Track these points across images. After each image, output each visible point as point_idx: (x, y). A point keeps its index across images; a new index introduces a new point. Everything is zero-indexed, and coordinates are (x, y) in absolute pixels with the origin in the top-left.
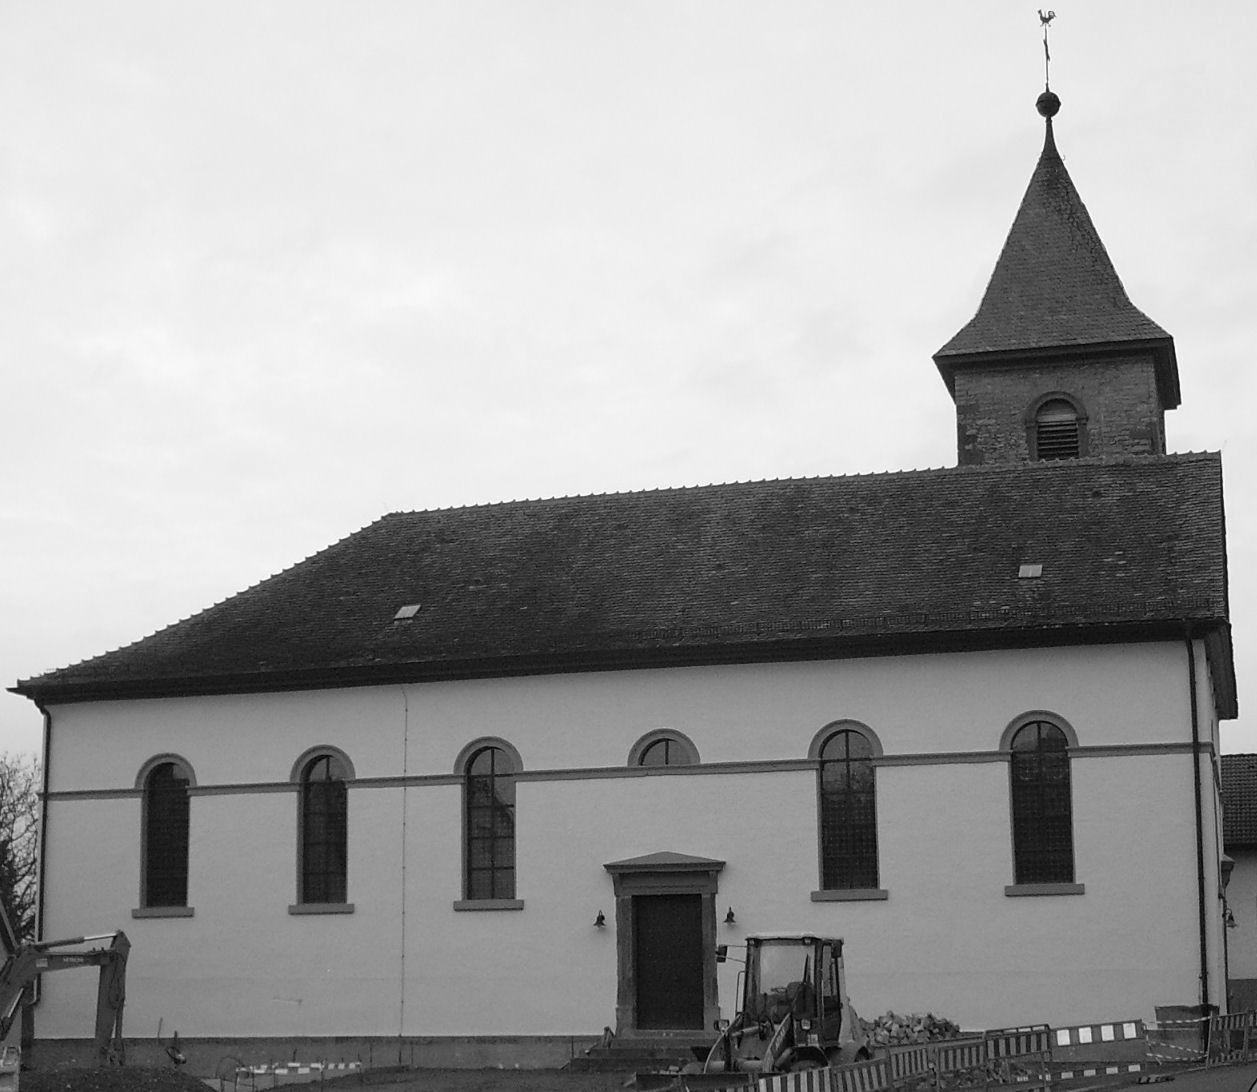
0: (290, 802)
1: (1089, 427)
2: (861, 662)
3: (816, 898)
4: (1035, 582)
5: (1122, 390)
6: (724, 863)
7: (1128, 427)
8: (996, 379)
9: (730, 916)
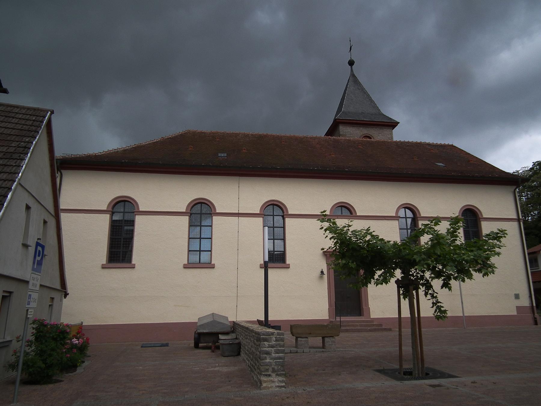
2: (286, 179)
3: (104, 267)
5: (384, 135)
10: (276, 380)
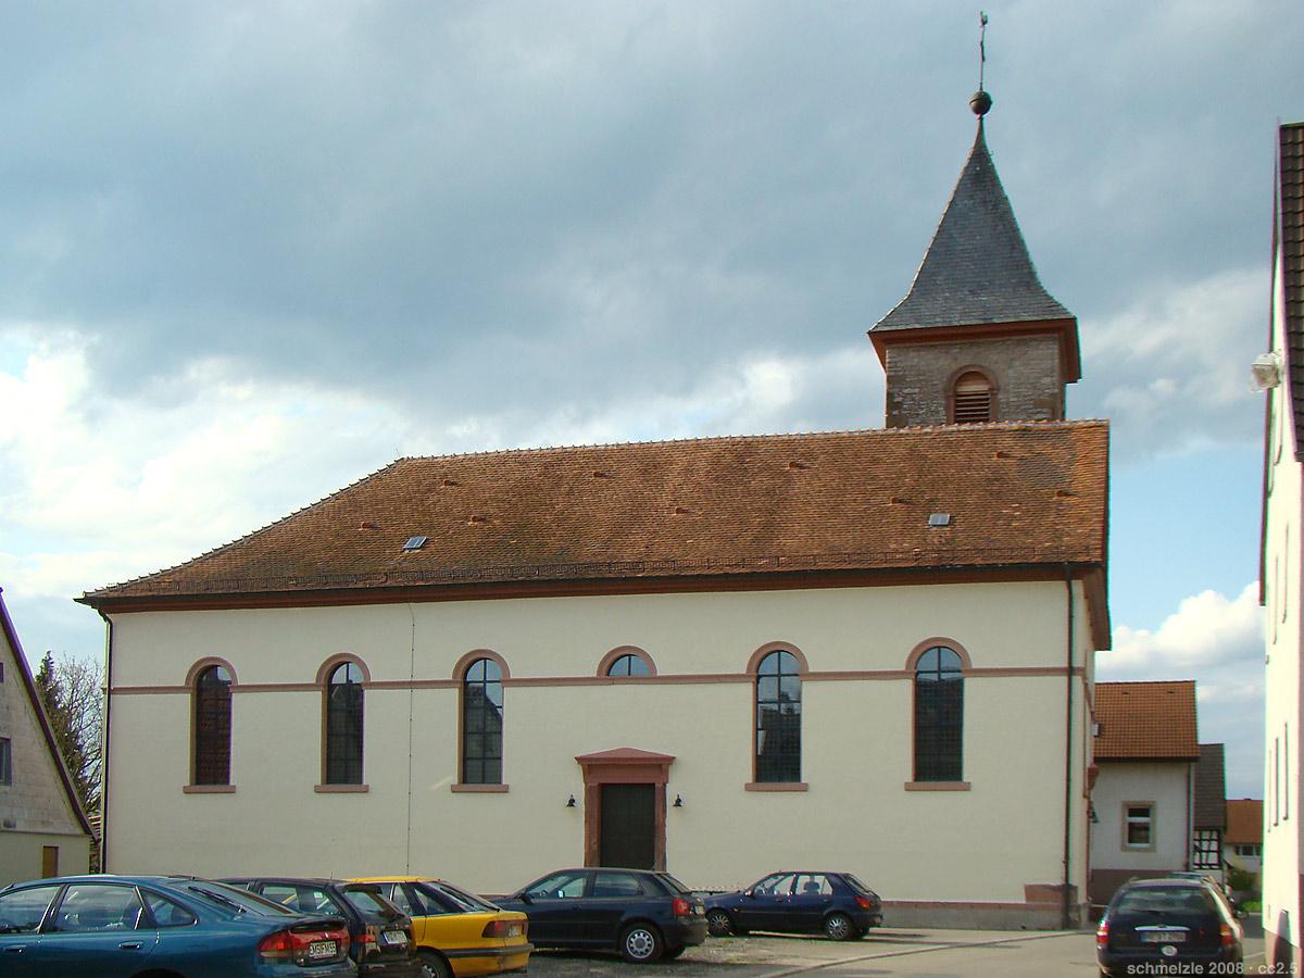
6: (673, 758)
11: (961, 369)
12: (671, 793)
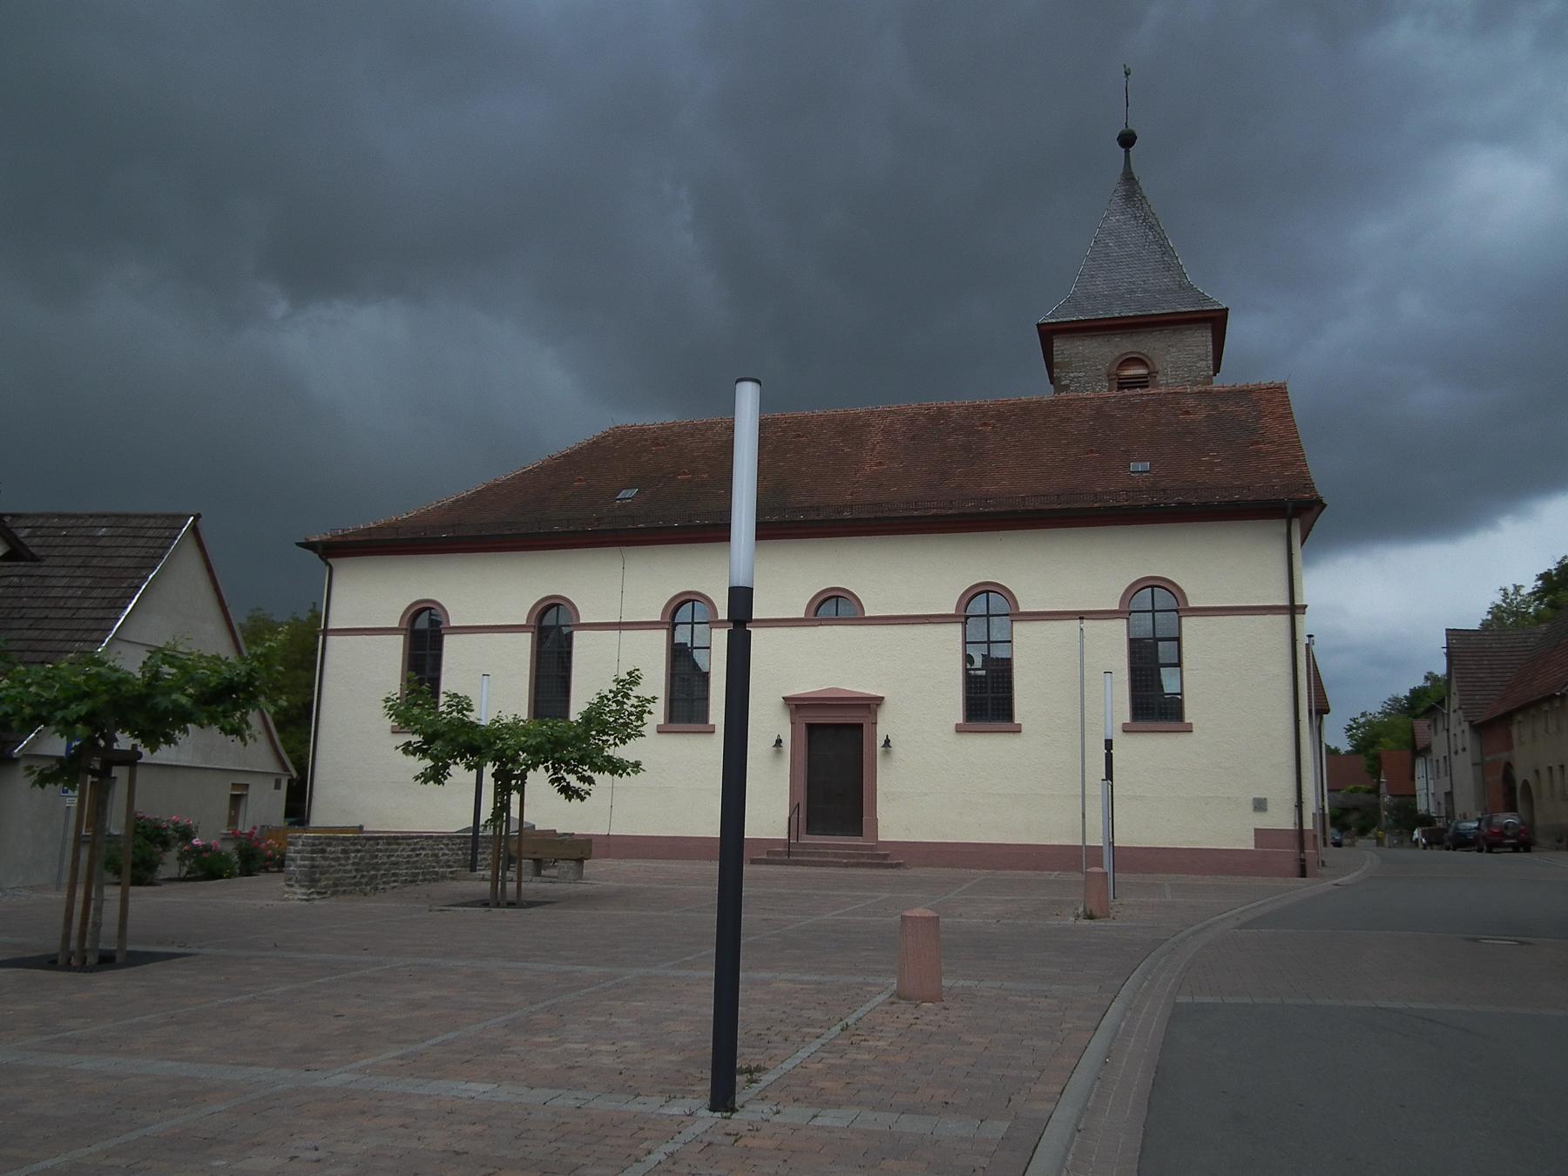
0: (525, 641)
1: (1158, 378)
3: (959, 730)
4: (1144, 474)
5: (1184, 350)
6: (883, 698)
7: (1190, 379)
8: (1086, 342)
9: (887, 742)
10: (298, 891)
11: (1122, 355)
12: (882, 732)
